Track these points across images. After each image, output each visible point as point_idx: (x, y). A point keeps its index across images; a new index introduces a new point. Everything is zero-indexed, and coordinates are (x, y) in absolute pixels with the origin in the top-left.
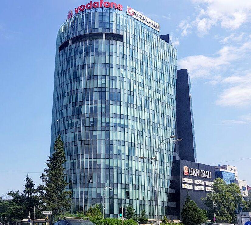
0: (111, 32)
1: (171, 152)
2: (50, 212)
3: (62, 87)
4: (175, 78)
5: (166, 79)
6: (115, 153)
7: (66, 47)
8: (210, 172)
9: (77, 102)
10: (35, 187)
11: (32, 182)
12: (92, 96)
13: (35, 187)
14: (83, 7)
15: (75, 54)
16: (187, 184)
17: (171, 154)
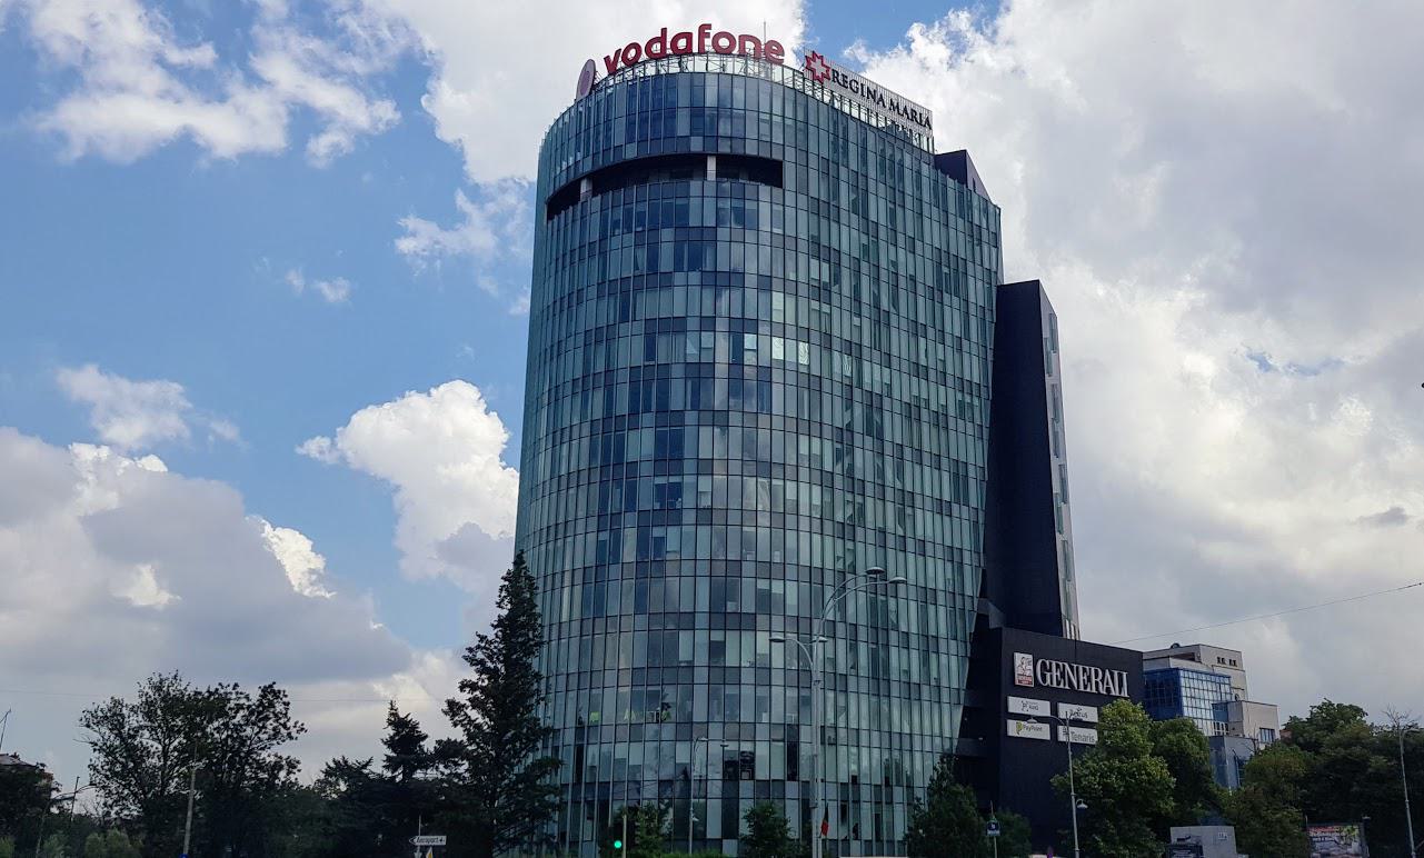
1: (968, 601)
2: (440, 837)
3: (555, 360)
4: (988, 318)
5: (953, 324)
7: (571, 208)
9: (607, 416)
10: (429, 746)
11: (415, 727)
13: (429, 746)
14: (632, 53)
15: (603, 238)
16: (1027, 719)
17: (968, 607)
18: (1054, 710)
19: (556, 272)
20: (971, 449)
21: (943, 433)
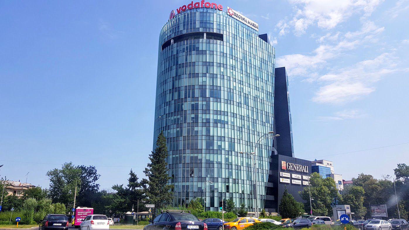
0: (211, 31)
1: (270, 148)
3: (165, 84)
4: (273, 76)
5: (265, 77)
6: (215, 148)
8: (307, 167)
10: (139, 181)
12: (193, 93)
13: (139, 181)
14: (184, 8)
15: (177, 53)
16: (284, 178)
17: (270, 149)
18: (291, 176)
19: (165, 63)
20: (269, 108)
21: (240, 108)
